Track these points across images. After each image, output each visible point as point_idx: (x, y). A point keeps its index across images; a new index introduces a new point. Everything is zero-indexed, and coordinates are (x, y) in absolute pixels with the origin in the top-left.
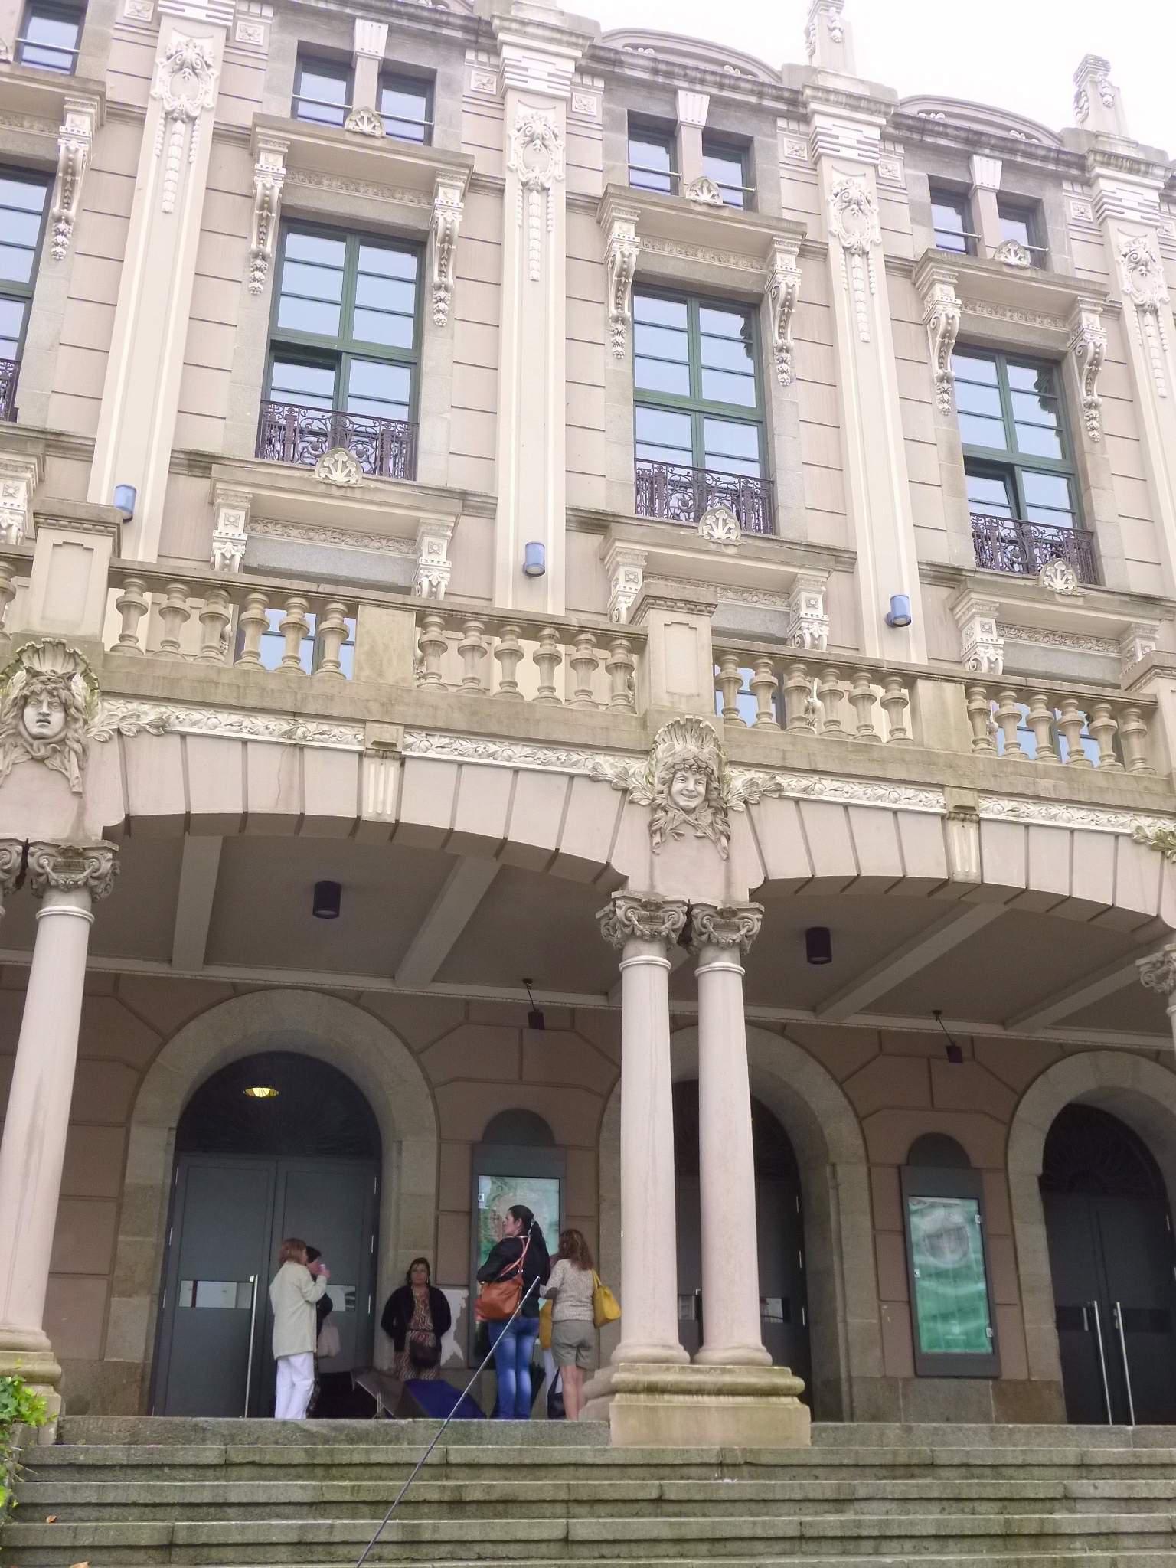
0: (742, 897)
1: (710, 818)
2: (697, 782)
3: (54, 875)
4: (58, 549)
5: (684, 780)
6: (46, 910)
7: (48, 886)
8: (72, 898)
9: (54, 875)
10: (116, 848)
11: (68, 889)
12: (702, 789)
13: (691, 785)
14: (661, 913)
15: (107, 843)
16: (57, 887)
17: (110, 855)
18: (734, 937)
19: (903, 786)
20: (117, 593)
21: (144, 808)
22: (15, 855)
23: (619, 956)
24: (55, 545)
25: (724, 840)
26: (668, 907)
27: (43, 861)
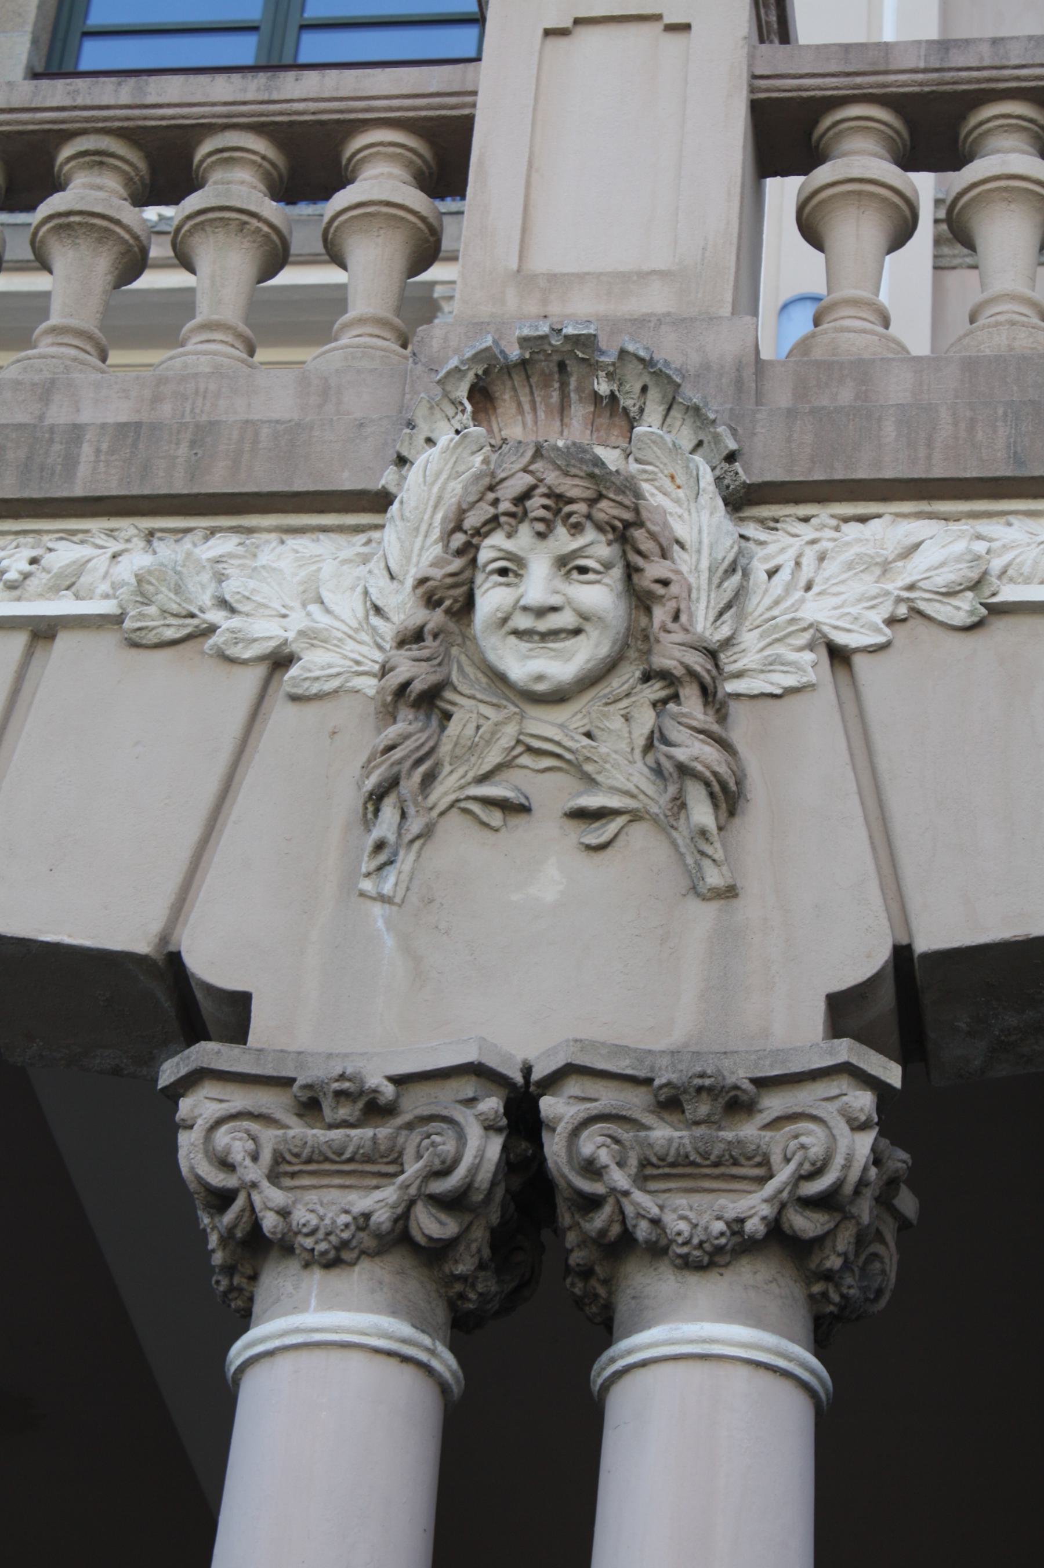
0: (797, 1031)
1: (646, 720)
2: (569, 566)
3: (272, 1196)
4: (554, 42)
5: (510, 570)
6: (264, 1332)
7: (256, 1247)
8: (360, 1278)
9: (271, 1196)
10: (893, 1074)
11: (707, 1259)
12: (600, 596)
13: (539, 583)
14: (748, 1131)
15: (845, 1050)
16: (658, 1250)
17: (864, 1101)
18: (362, 1202)
19: (824, 513)
20: (783, 192)
21: (942, 928)
22: (474, 1133)
23: (604, 1327)
24: (548, 33)
25: (702, 812)
26: (774, 1104)
27: (232, 1141)
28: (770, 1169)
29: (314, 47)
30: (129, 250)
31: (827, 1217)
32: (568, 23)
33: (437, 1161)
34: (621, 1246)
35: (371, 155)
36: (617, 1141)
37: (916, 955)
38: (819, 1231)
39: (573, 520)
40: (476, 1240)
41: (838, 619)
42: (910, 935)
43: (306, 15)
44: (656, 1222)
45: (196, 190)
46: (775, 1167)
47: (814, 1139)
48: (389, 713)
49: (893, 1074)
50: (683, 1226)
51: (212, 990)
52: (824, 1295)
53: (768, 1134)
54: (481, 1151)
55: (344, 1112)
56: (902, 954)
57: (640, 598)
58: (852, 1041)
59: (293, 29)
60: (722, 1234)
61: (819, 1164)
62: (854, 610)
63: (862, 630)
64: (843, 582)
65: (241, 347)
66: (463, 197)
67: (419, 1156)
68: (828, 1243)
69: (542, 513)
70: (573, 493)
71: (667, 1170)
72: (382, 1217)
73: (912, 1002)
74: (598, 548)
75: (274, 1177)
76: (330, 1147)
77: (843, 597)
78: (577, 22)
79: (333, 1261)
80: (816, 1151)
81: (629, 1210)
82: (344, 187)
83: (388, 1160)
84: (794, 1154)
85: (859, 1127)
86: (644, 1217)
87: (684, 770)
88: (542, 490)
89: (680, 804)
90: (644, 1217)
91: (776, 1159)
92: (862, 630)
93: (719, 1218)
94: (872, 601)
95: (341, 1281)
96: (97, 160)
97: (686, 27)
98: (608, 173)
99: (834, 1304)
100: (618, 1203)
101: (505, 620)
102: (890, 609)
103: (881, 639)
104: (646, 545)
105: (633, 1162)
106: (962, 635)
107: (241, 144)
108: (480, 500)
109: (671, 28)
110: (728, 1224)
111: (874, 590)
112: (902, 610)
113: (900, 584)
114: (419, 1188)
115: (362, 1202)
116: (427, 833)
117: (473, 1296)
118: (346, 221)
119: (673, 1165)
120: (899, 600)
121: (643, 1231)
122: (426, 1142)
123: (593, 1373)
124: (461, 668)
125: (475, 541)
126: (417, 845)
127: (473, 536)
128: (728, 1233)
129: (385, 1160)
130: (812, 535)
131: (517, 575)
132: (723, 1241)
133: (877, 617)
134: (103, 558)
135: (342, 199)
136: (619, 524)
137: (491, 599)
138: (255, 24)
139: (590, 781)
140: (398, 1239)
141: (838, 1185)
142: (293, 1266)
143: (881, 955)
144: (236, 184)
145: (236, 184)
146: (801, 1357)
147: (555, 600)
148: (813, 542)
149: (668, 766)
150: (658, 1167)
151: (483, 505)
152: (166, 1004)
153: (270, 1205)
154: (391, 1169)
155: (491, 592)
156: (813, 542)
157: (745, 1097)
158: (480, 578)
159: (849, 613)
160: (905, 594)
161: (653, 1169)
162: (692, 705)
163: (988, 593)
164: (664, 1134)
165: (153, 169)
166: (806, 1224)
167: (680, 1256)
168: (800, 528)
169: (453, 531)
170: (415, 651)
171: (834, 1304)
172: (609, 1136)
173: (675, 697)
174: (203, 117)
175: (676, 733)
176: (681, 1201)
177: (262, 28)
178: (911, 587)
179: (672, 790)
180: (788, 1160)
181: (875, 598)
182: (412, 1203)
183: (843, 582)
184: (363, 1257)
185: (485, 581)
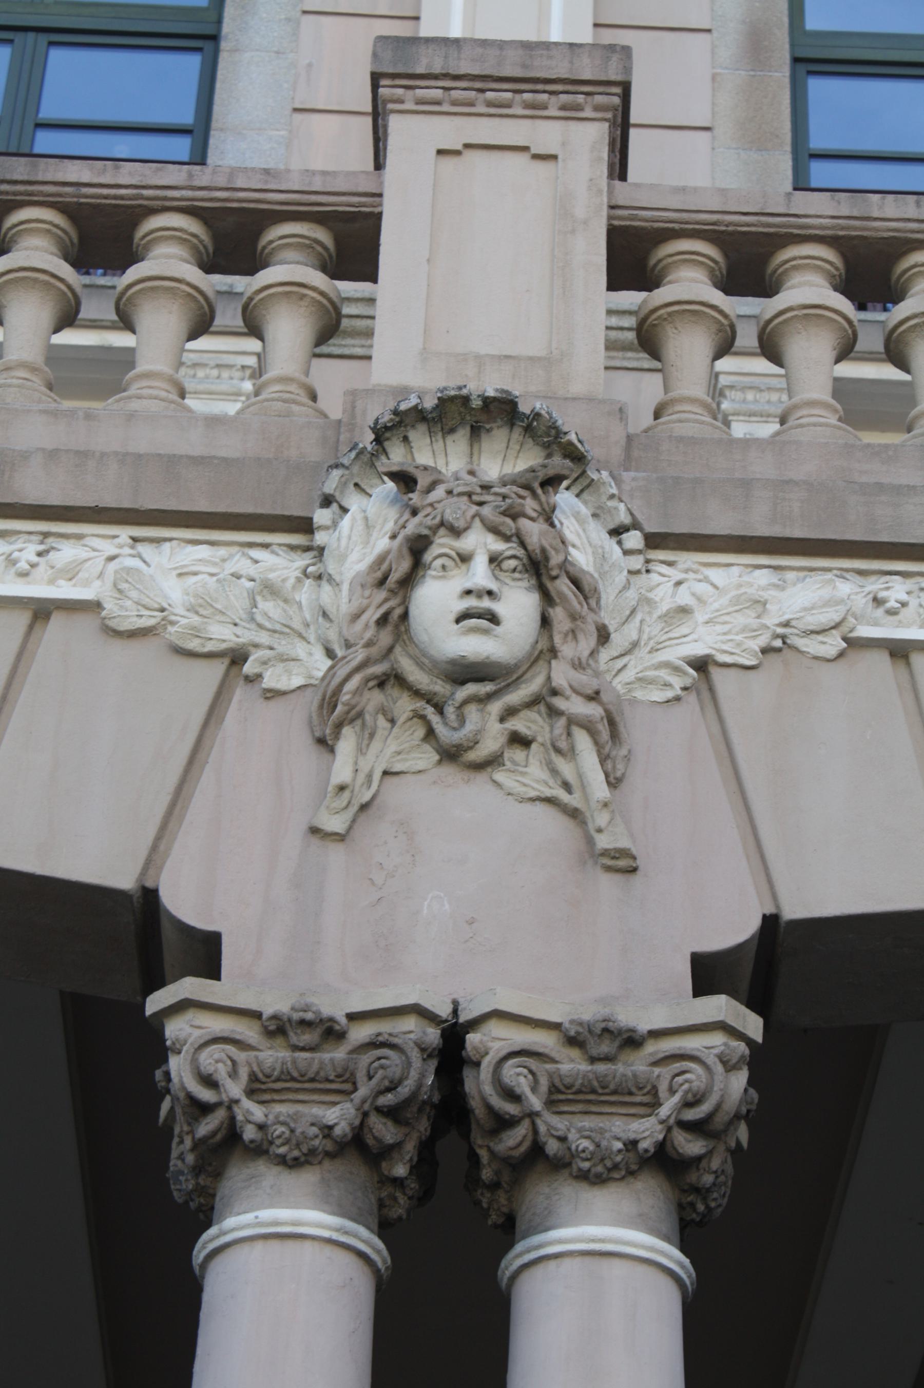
4: (449, 163)
6: (235, 1223)
11: (600, 1173)
24: (440, 152)
28: (354, 1083)
29: (45, 141)
30: (204, 314)
31: (704, 1143)
32: (459, 147)
33: (690, 1095)
35: (162, 237)
37: (783, 925)
38: (703, 1151)
40: (409, 1152)
42: (778, 907)
43: (41, 115)
44: (563, 1139)
45: (136, 262)
47: (696, 1076)
50: (585, 1143)
52: (692, 1205)
54: (420, 1076)
55: (307, 1038)
56: (770, 922)
58: (728, 997)
59: (30, 126)
61: (698, 1096)
62: (739, 638)
64: (728, 614)
65: (706, 414)
66: (375, 280)
67: (672, 1091)
68: (704, 1164)
71: (571, 1097)
73: (771, 966)
75: (251, 1093)
76: (561, 1080)
78: (467, 146)
79: (292, 1164)
81: (542, 1129)
83: (344, 1078)
84: (376, 1073)
85: (729, 1066)
86: (250, 1122)
90: (250, 1122)
91: (361, 1076)
93: (618, 1139)
94: (753, 632)
96: (690, 258)
97: (554, 157)
98: (489, 272)
99: (698, 1214)
100: (533, 1124)
102: (767, 640)
106: (830, 664)
107: (693, 249)
109: (536, 157)
110: (625, 1144)
111: (755, 623)
112: (778, 643)
113: (777, 621)
114: (372, 1104)
115: (331, 1115)
117: (701, 1207)
118: (273, 295)
119: (579, 1092)
120: (777, 636)
121: (552, 1147)
123: (195, 1253)
128: (321, 1136)
129: (340, 1079)
130: (114, 551)
133: (756, 645)
134: (98, 560)
135: (134, 273)
138: (190, 128)
140: (663, 1161)
141: (710, 1116)
142: (261, 1167)
143: (753, 925)
144: (169, 259)
145: (169, 259)
146: (672, 1256)
148: (112, 558)
150: (264, 1083)
152: (143, 938)
154: (347, 1087)
156: (112, 558)
157: (337, 1027)
159: (731, 640)
160: (780, 630)
161: (560, 1095)
163: (847, 629)
164: (273, 1056)
165: (848, 270)
166: (690, 1146)
167: (278, 1155)
168: (664, 569)
171: (698, 1214)
174: (687, 223)
176: (587, 1122)
177: (807, 156)
178: (786, 624)
180: (370, 1078)
181: (755, 631)
182: (365, 1115)
183: (728, 614)
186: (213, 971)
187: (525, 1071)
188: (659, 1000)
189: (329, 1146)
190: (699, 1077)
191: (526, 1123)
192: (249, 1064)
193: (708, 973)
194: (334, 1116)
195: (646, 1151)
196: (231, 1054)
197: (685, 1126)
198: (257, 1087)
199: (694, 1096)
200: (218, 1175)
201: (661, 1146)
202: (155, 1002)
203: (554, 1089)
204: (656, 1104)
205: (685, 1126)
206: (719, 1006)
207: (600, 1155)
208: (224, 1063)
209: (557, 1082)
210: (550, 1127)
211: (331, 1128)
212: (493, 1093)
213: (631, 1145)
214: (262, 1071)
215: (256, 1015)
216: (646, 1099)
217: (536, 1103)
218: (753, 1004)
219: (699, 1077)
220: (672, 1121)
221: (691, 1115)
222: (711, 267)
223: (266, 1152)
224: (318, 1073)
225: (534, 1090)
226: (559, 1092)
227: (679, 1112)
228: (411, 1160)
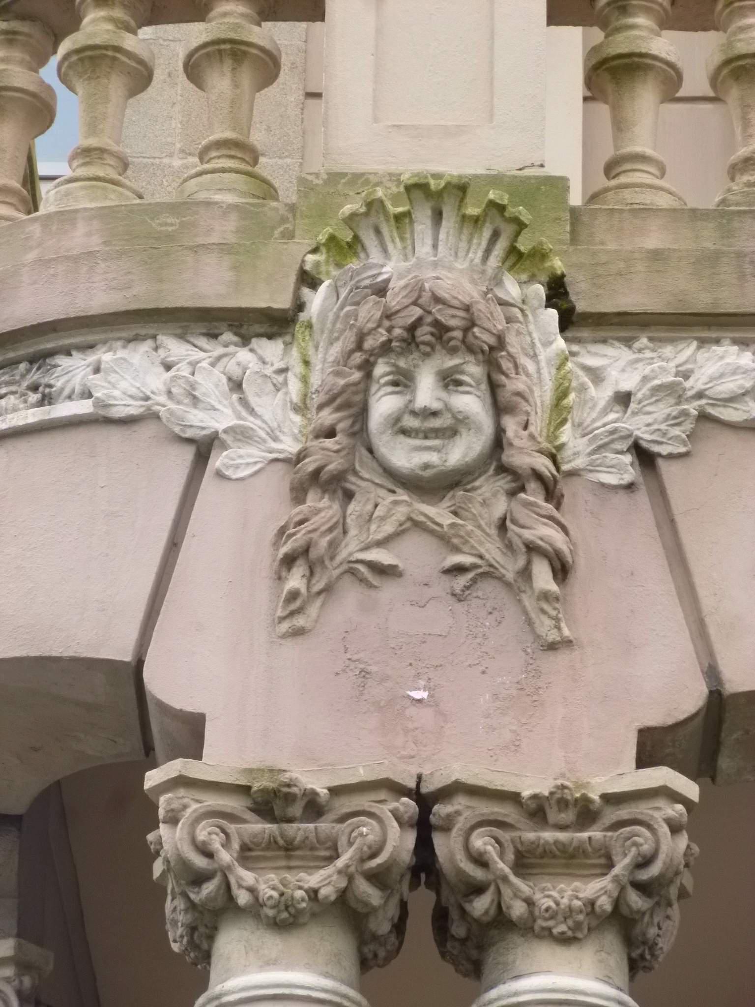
2: (450, 381)
11: (285, 919)
12: (471, 403)
25: (543, 577)
28: (336, 850)
33: (365, 849)
34: (502, 922)
36: (223, 831)
39: (452, 343)
41: (652, 434)
44: (252, 890)
46: (615, 858)
47: (644, 840)
48: (299, 493)
49: (691, 789)
51: (164, 708)
53: (338, 826)
54: (400, 843)
55: (568, 816)
57: (500, 408)
60: (303, 900)
62: (663, 427)
63: (670, 442)
67: (350, 844)
69: (428, 338)
70: (452, 323)
72: (605, 904)
74: (474, 370)
77: (655, 416)
80: (646, 848)
82: (705, 29)
87: (531, 548)
88: (429, 319)
89: (526, 573)
91: (343, 841)
92: (670, 442)
93: (300, 888)
95: (295, 944)
101: (398, 420)
103: (682, 450)
104: (506, 365)
105: (236, 846)
108: (379, 326)
115: (313, 879)
116: (327, 590)
122: (628, 843)
124: (361, 461)
125: (372, 359)
126: (322, 597)
127: (371, 355)
131: (406, 386)
132: (304, 905)
136: (486, 348)
137: (384, 405)
139: (456, 550)
147: (436, 405)
149: (517, 542)
151: (381, 330)
153: (244, 884)
155: (384, 399)
158: (374, 388)
159: (659, 430)
162: (534, 495)
164: (258, 827)
169: (352, 352)
170: (329, 443)
172: (219, 827)
173: (523, 489)
175: (521, 514)
179: (521, 562)
184: (611, 940)
185: (379, 390)
186: (196, 753)
187: (218, 830)
188: (613, 772)
189: (316, 908)
190: (646, 840)
191: (219, 875)
192: (513, 841)
193: (652, 747)
194: (671, 892)
195: (326, 897)
196: (493, 834)
197: (639, 886)
198: (248, 853)
199: (370, 847)
200: (211, 938)
201: (343, 896)
202: (153, 778)
203: (245, 848)
204: (611, 865)
205: (639, 886)
206: (661, 776)
207: (286, 904)
208: (217, 834)
209: (247, 840)
210: (239, 879)
211: (316, 892)
212: (464, 859)
213: (313, 894)
214: (558, 849)
215: (513, 798)
216: (326, 853)
217: (502, 867)
218: (694, 777)
219: (646, 840)
220: (625, 880)
221: (644, 875)
222: (729, 206)
223: (532, 929)
224: (303, 842)
225: (502, 856)
226: (250, 850)
227: (632, 872)
228: (392, 919)
